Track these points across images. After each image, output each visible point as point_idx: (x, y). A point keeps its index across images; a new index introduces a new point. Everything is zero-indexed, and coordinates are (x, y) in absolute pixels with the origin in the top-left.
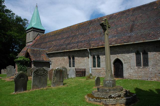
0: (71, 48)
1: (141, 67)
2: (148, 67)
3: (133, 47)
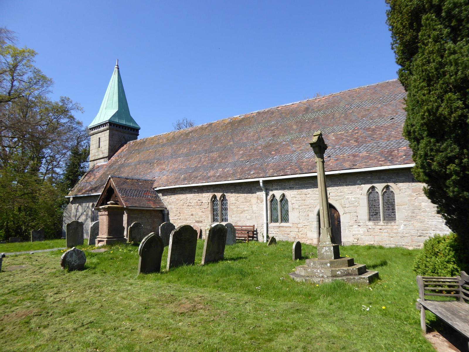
0: (219, 178)
1: (381, 223)
2: (395, 222)
3: (362, 179)
